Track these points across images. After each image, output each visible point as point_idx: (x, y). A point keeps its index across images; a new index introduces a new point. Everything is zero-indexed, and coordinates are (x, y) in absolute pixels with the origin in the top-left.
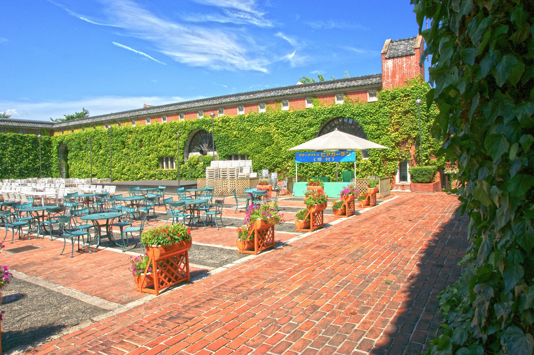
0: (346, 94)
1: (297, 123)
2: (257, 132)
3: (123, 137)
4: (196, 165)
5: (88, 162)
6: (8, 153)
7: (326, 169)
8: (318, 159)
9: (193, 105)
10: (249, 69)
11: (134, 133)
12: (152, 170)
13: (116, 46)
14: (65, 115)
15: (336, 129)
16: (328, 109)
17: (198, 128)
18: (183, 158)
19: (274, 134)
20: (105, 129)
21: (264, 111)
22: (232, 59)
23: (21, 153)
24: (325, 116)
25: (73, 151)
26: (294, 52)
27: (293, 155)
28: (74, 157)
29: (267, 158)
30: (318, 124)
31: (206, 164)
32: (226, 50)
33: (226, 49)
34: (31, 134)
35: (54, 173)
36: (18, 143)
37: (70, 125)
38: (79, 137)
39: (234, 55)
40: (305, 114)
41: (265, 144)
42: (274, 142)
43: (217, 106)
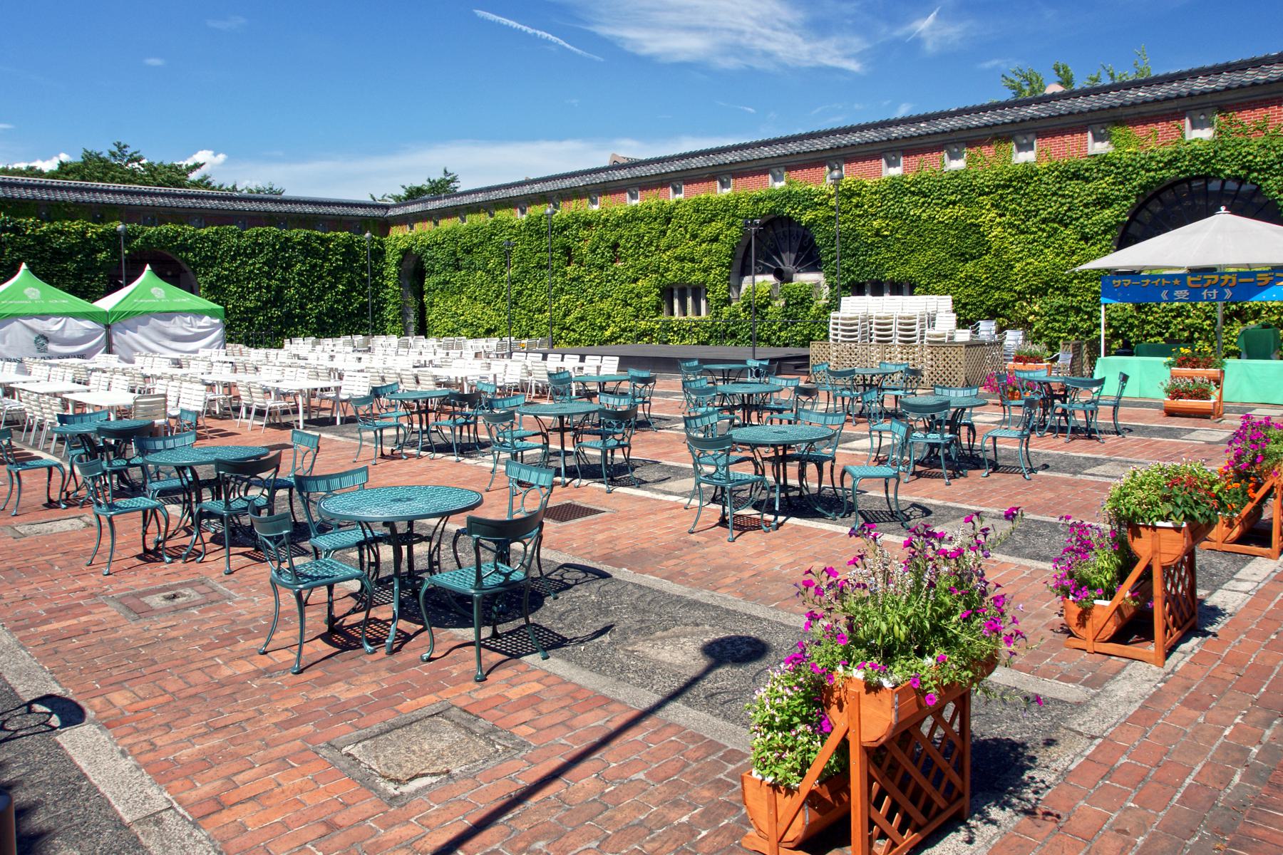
0: (1223, 109)
1: (1063, 196)
2: (943, 222)
3: (568, 237)
4: (765, 307)
5: (475, 299)
6: (294, 278)
7: (1150, 322)
8: (1177, 293)
9: (756, 154)
10: (812, 65)
11: (598, 225)
12: (643, 319)
13: (482, 20)
14: (403, 187)
15: (1223, 208)
16: (1162, 156)
17: (772, 211)
18: (729, 291)
19: (991, 227)
20: (518, 218)
21: (958, 164)
22: (768, 39)
23: (320, 277)
24: (1152, 174)
25: (438, 273)
26: (935, 13)
27: (1047, 283)
28: (440, 286)
29: (969, 291)
30: (1126, 198)
31: (793, 305)
32: (752, 18)
33: (753, 14)
34: (341, 231)
35: (389, 325)
36: (314, 253)
37: (430, 208)
38: (454, 237)
39: (775, 29)
40: (1087, 170)
41: (963, 254)
42: (990, 248)
43: (825, 154)
